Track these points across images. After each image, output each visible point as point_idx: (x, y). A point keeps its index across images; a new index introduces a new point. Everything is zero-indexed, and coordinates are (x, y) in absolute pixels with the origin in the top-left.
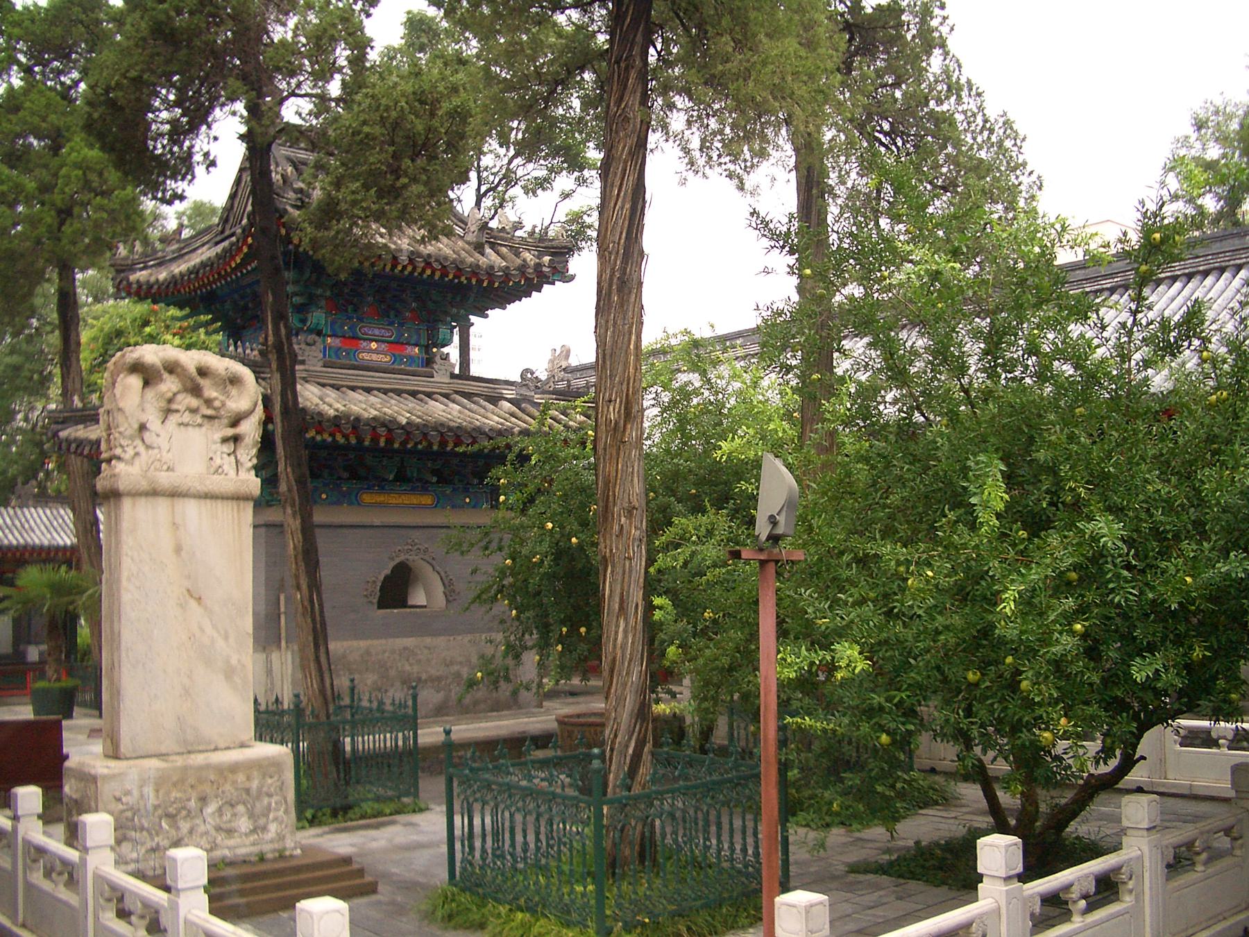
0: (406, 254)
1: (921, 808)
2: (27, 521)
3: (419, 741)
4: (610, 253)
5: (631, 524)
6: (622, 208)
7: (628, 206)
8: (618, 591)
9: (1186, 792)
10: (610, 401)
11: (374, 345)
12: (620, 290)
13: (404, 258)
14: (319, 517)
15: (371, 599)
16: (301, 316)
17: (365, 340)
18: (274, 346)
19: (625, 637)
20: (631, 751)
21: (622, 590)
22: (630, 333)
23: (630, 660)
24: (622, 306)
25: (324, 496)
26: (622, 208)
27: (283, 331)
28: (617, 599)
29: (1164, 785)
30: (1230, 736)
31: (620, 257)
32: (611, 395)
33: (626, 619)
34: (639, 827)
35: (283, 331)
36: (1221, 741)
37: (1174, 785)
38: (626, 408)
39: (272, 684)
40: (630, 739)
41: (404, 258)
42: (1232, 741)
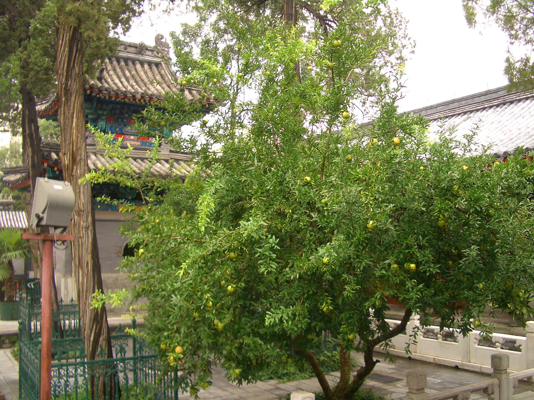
0: (140, 94)
1: (333, 371)
2: (20, 217)
3: (109, 323)
4: (60, 76)
5: (80, 219)
6: (64, 51)
7: (67, 49)
8: (77, 255)
9: (478, 370)
10: (65, 154)
11: (132, 137)
12: (66, 94)
13: (138, 96)
14: (97, 217)
15: (119, 254)
16: (95, 124)
17: (127, 135)
18: (28, 135)
19: (83, 279)
20: (92, 339)
21: (79, 256)
22: (73, 117)
23: (86, 292)
24: (67, 103)
25: (99, 207)
26: (64, 51)
27: (33, 128)
28: (77, 259)
29: (468, 366)
30: (501, 341)
31: (65, 77)
32: (65, 151)
33: (82, 269)
34: (102, 379)
35: (33, 128)
36: (497, 344)
37: (473, 366)
38: (73, 157)
39: (68, 292)
40: (91, 333)
41: (138, 96)
42: (502, 344)
